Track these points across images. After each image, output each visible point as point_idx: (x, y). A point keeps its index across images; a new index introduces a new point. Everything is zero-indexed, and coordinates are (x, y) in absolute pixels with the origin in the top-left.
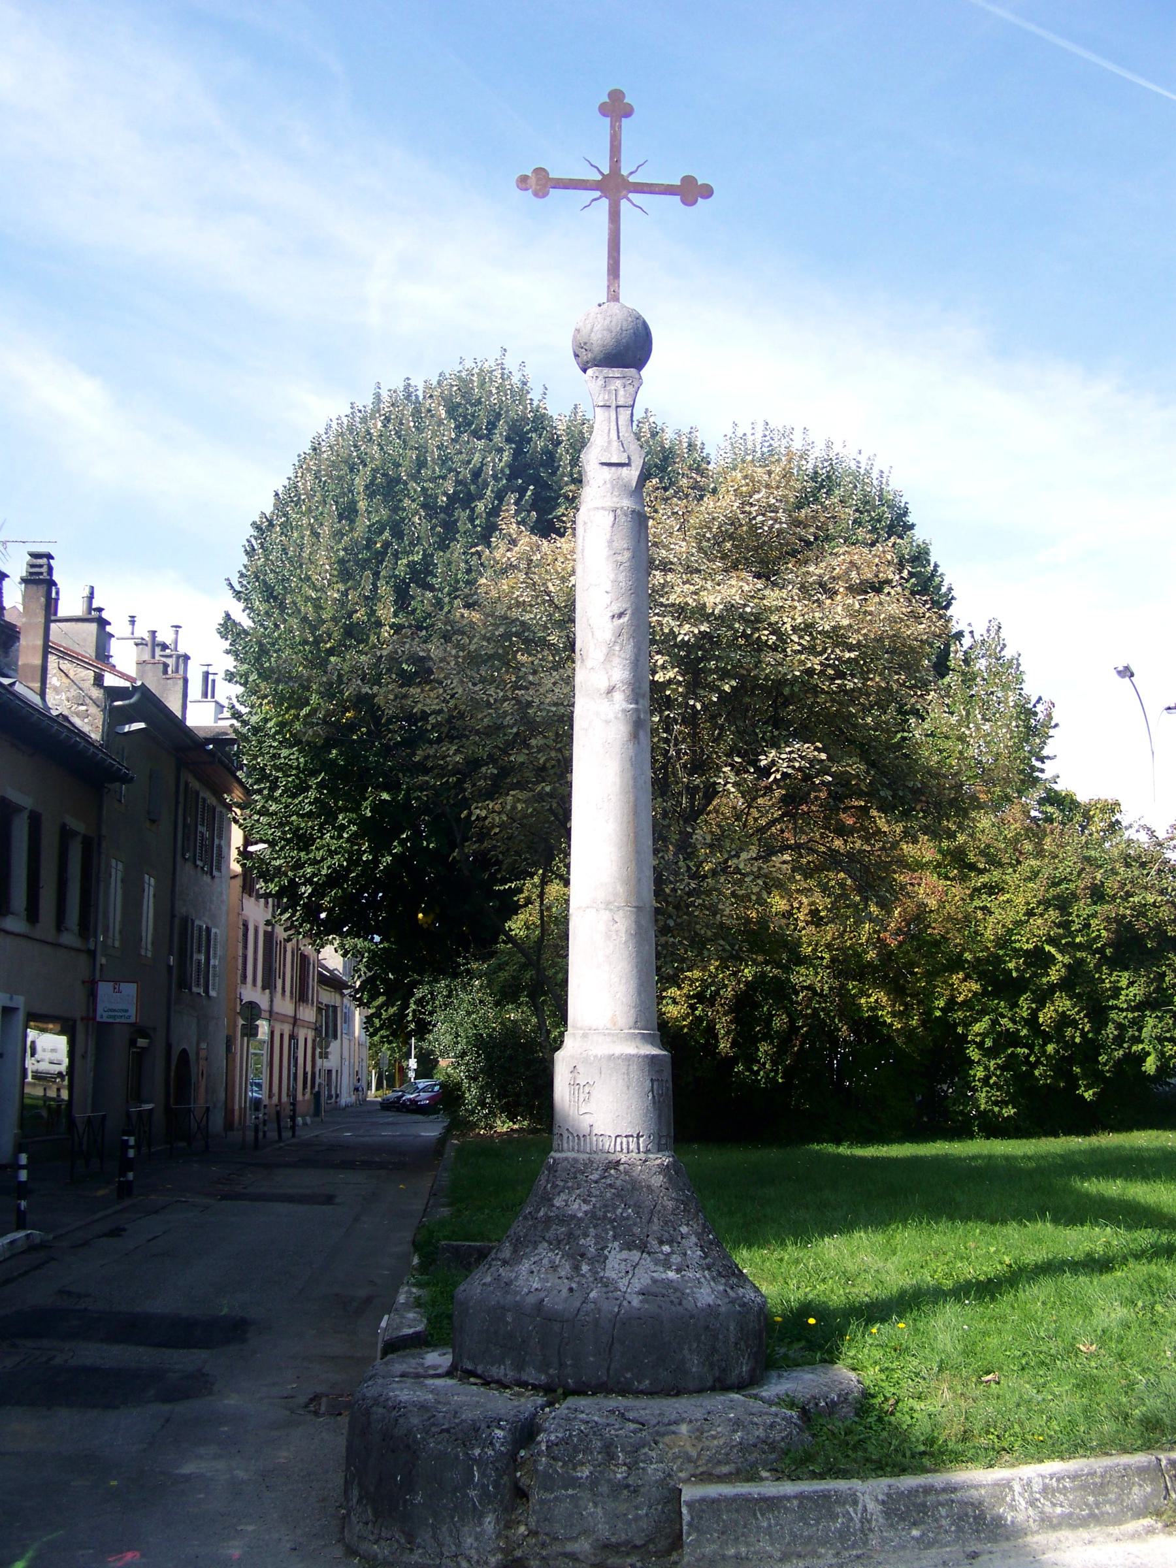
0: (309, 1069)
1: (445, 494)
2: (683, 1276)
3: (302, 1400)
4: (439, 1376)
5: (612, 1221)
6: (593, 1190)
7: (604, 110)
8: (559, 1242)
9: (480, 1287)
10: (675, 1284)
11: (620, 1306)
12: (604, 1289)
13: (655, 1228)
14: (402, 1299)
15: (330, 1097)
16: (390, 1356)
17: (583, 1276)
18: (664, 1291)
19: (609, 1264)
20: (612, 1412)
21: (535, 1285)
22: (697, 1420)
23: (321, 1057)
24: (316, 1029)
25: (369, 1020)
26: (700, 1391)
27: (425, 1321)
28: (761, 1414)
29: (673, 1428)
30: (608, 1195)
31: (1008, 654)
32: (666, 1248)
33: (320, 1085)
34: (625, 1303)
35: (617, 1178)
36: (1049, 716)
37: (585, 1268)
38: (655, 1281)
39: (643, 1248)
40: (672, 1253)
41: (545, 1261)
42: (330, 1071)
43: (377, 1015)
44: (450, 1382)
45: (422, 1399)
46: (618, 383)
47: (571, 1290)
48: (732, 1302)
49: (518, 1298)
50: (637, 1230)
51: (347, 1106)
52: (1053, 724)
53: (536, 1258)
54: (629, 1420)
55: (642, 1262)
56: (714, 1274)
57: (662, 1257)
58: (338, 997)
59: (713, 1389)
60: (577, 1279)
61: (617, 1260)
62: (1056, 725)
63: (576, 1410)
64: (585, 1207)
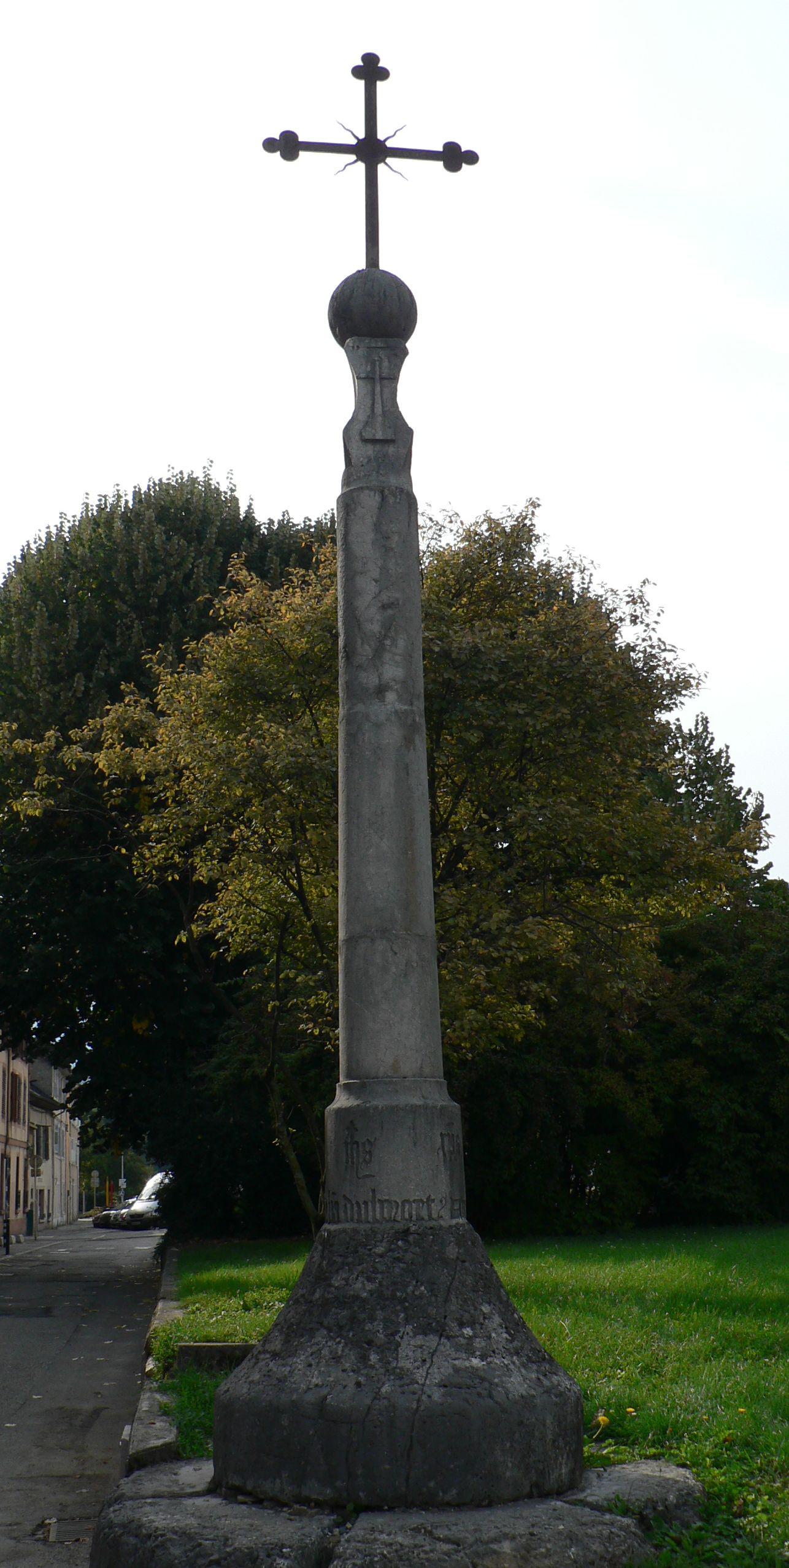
0: (21, 1188)
1: (156, 595)
2: (489, 1363)
3: (29, 1527)
4: (198, 1495)
5: (402, 1301)
6: (378, 1266)
7: (357, 72)
8: (341, 1328)
9: (246, 1386)
10: (482, 1373)
11: (419, 1401)
12: (398, 1382)
13: (453, 1308)
14: (144, 1406)
15: (42, 1216)
16: (136, 1474)
17: (372, 1367)
18: (469, 1382)
19: (402, 1353)
20: (417, 1530)
21: (314, 1381)
22: (521, 1536)
23: (33, 1175)
24: (28, 1148)
25: (83, 1131)
26: (515, 1500)
27: (175, 1430)
28: (593, 1524)
29: (495, 1547)
30: (397, 1270)
31: (715, 748)
32: (468, 1331)
33: (32, 1204)
34: (424, 1398)
35: (406, 1251)
36: (760, 808)
37: (374, 1358)
38: (457, 1370)
39: (441, 1332)
40: (475, 1336)
41: (325, 1352)
42: (42, 1191)
43: (92, 1125)
44: (214, 1501)
45: (182, 1525)
46: (382, 353)
47: (358, 1384)
48: (548, 1392)
49: (295, 1397)
50: (432, 1311)
51: (58, 1226)
52: (763, 815)
53: (315, 1348)
54: (439, 1539)
55: (441, 1348)
56: (524, 1359)
57: (462, 1341)
58: (48, 1117)
59: (530, 1496)
60: (364, 1372)
61: (410, 1349)
62: (768, 816)
63: (373, 1530)
64: (370, 1286)
